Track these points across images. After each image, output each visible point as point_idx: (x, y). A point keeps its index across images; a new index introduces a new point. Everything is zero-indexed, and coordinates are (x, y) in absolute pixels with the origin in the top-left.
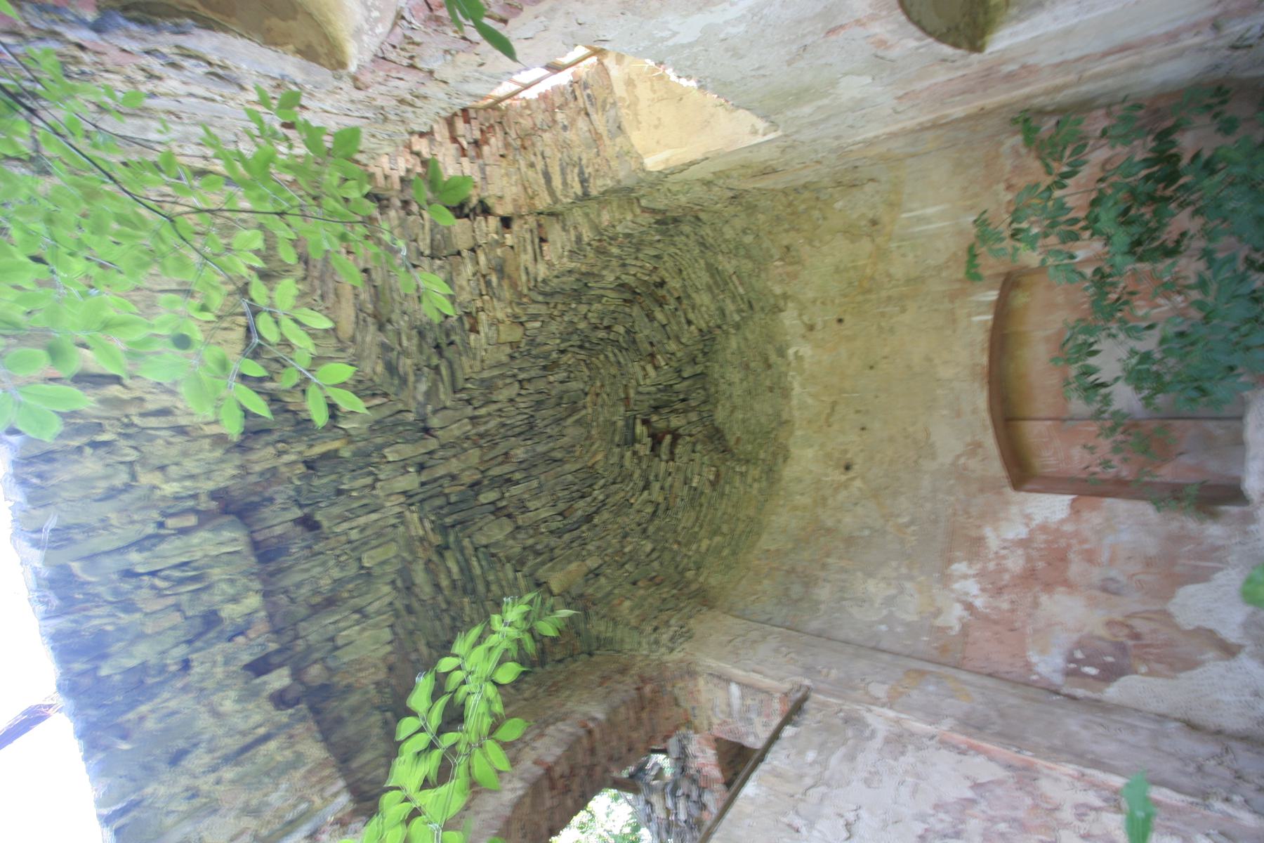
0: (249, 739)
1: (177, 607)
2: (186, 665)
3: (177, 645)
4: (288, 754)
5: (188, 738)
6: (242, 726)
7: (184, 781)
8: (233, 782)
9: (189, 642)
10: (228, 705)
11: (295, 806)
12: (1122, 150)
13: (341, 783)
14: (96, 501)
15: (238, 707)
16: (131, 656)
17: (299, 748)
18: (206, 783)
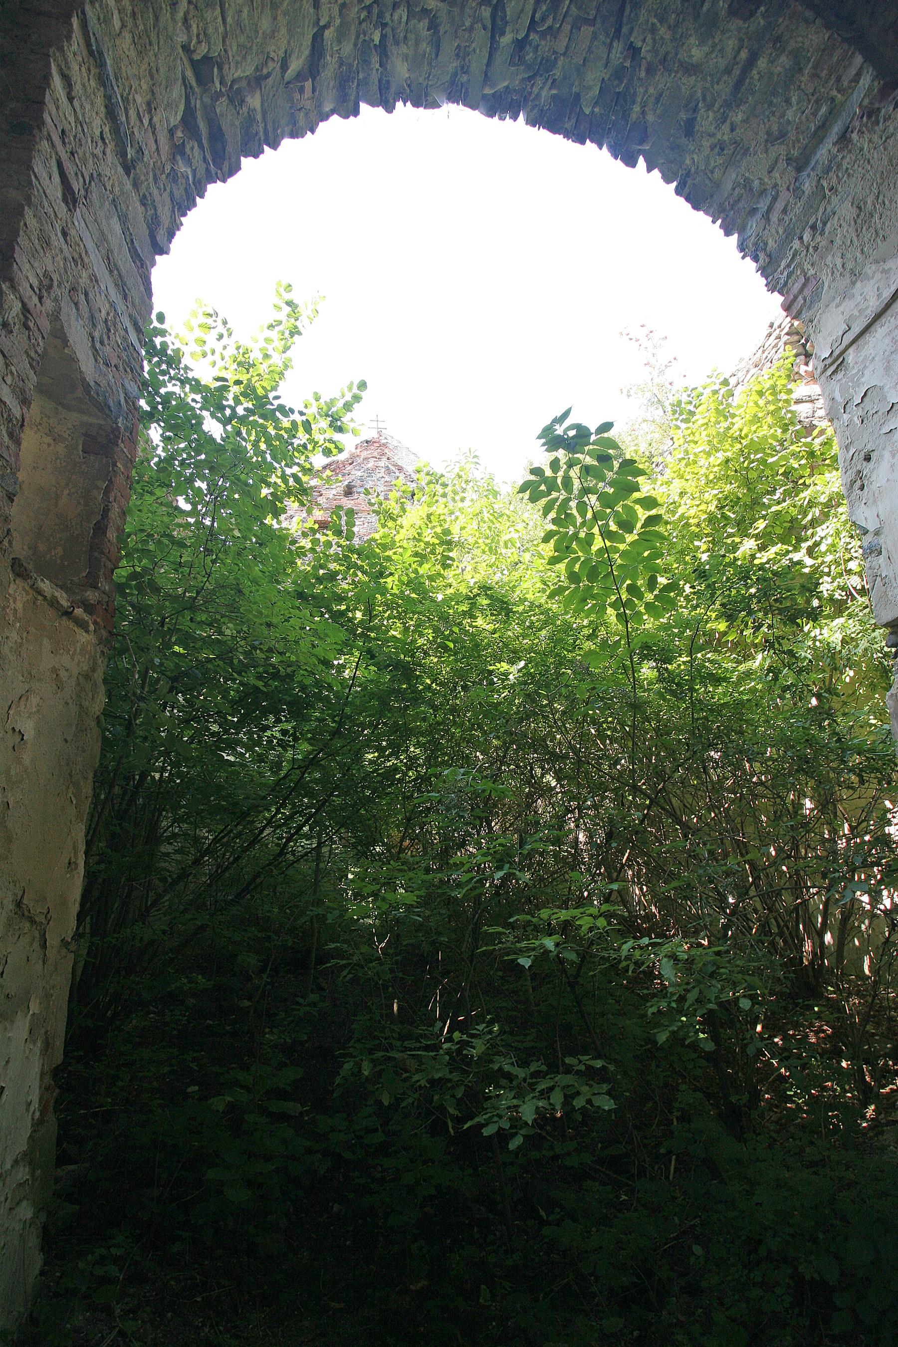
0: (736, 72)
1: (576, 26)
2: (633, 51)
3: (610, 47)
4: (784, 60)
5: (686, 106)
6: (722, 63)
7: (706, 143)
8: (746, 121)
9: (617, 34)
10: (697, 54)
11: (814, 114)
12: (180, 162)
13: (859, 59)
14: (437, 56)
15: (706, 49)
16: (590, 88)
17: (792, 45)
18: (724, 134)
